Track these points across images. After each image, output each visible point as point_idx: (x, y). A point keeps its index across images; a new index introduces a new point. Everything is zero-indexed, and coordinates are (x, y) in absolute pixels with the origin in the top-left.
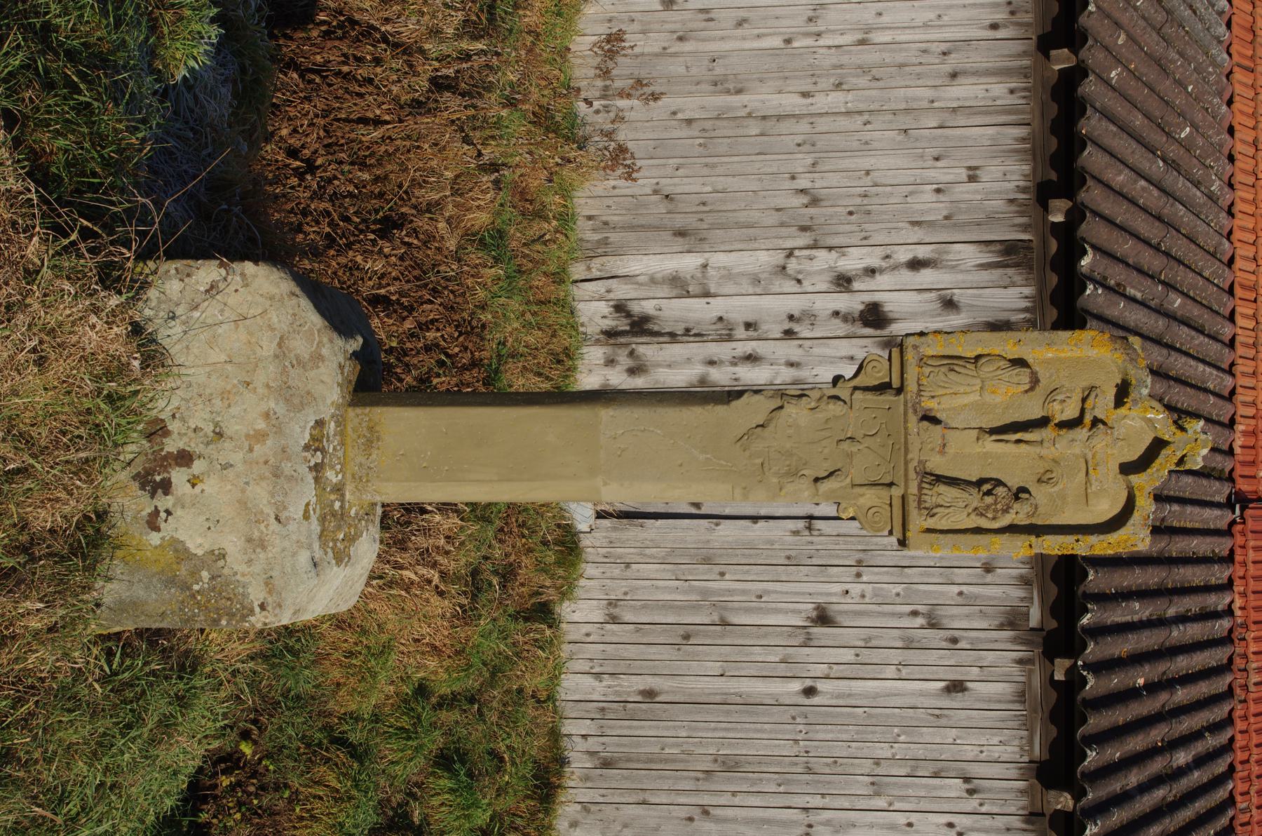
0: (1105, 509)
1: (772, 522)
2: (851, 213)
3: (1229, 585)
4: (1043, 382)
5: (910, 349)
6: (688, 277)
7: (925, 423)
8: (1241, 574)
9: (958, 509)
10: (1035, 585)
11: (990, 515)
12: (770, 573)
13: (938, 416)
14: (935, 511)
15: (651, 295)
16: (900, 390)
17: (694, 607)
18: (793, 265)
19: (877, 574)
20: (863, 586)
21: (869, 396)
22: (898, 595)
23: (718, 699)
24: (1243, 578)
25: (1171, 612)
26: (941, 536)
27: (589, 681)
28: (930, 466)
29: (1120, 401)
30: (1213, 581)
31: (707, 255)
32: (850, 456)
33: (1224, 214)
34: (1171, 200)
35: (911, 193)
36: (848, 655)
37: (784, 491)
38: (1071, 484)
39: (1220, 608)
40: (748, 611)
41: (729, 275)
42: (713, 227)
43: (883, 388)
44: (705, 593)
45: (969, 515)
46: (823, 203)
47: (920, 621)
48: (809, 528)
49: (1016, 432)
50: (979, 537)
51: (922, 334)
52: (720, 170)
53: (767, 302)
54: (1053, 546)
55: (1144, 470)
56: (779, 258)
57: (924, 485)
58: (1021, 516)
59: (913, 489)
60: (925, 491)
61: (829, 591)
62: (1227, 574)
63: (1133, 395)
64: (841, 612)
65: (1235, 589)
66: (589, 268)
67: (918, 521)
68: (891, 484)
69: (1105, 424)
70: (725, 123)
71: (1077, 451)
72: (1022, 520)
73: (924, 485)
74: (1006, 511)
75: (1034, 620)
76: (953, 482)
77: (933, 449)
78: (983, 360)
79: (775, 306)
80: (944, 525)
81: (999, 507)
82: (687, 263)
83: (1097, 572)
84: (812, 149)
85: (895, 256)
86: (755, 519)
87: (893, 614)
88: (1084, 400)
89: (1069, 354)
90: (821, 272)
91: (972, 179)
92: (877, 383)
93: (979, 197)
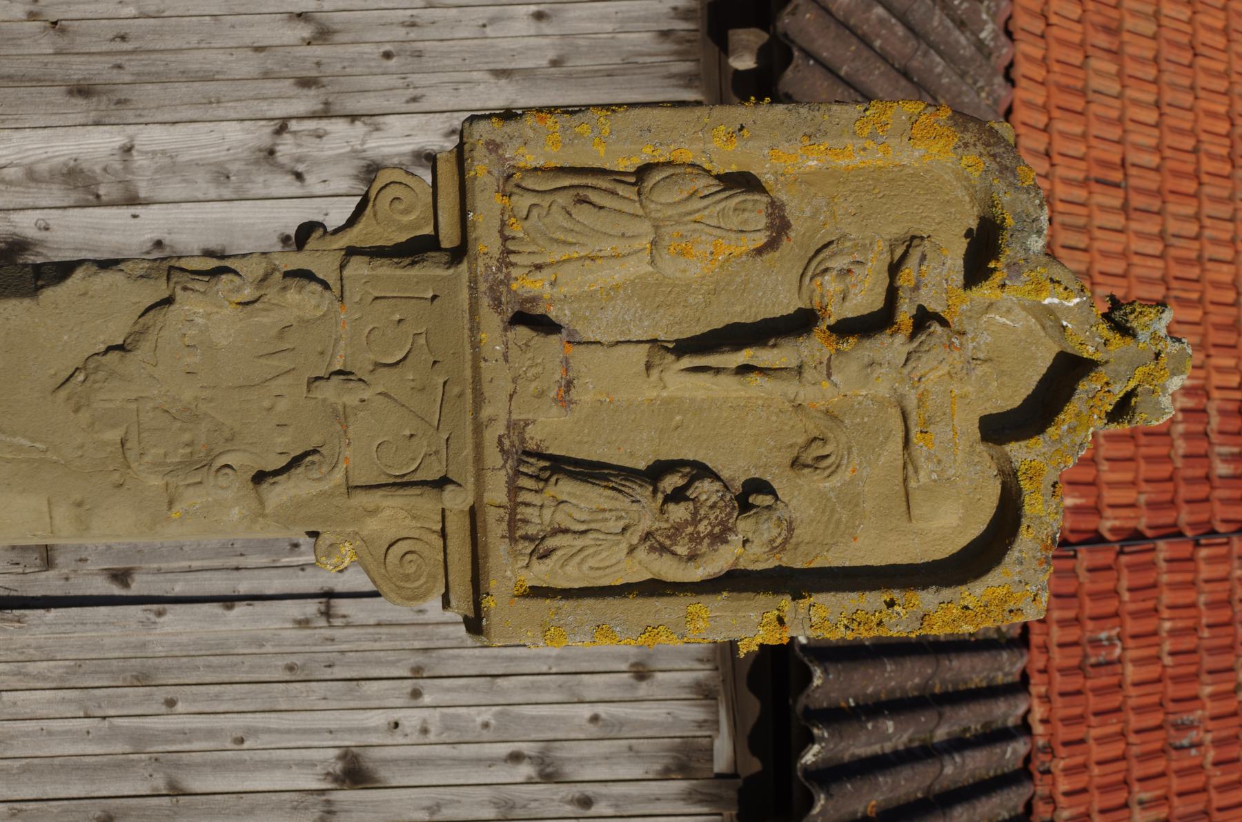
0: (950, 526)
1: (259, 606)
2: (388, 55)
3: (1022, 685)
4: (798, 228)
5: (480, 152)
6: (98, 169)
7: (523, 332)
8: (1040, 664)
9: (604, 537)
10: (722, 698)
11: (682, 550)
13: (553, 313)
14: (551, 543)
15: (29, 201)
16: (459, 254)
17: (121, 766)
18: (287, 148)
19: (449, 690)
20: (425, 713)
21: (385, 269)
22: (486, 725)
24: (1044, 671)
25: (941, 734)
26: (566, 605)
28: (536, 436)
29: (977, 268)
30: (1000, 678)
31: (131, 130)
32: (342, 416)
33: (999, 80)
34: (924, 46)
35: (493, 20)
37: (178, 508)
38: (870, 468)
39: (1011, 722)
40: (219, 767)
41: (172, 166)
42: (140, 79)
43: (416, 249)
44: (139, 739)
45: (632, 550)
46: (338, 38)
47: (525, 770)
48: (327, 614)
49: (738, 346)
50: (658, 603)
51: (508, 115)
53: (241, 213)
54: (754, 625)
55: (1041, 430)
57: (524, 482)
58: (755, 549)
59: (497, 493)
60: (525, 497)
61: (364, 724)
62: (1019, 666)
63: (1010, 252)
64: (386, 762)
65: (1034, 690)
67: (509, 570)
68: (442, 483)
69: (944, 323)
71: (882, 389)
72: (758, 558)
73: (524, 482)
74: (719, 538)
75: (722, 763)
76: (591, 472)
77: (541, 394)
78: (657, 176)
79: (261, 220)
80: (572, 577)
82: (96, 144)
83: (826, 671)
86: (229, 601)
87: (478, 761)
88: (894, 269)
89: (857, 161)
90: (337, 160)
92: (403, 238)
93: (609, 27)
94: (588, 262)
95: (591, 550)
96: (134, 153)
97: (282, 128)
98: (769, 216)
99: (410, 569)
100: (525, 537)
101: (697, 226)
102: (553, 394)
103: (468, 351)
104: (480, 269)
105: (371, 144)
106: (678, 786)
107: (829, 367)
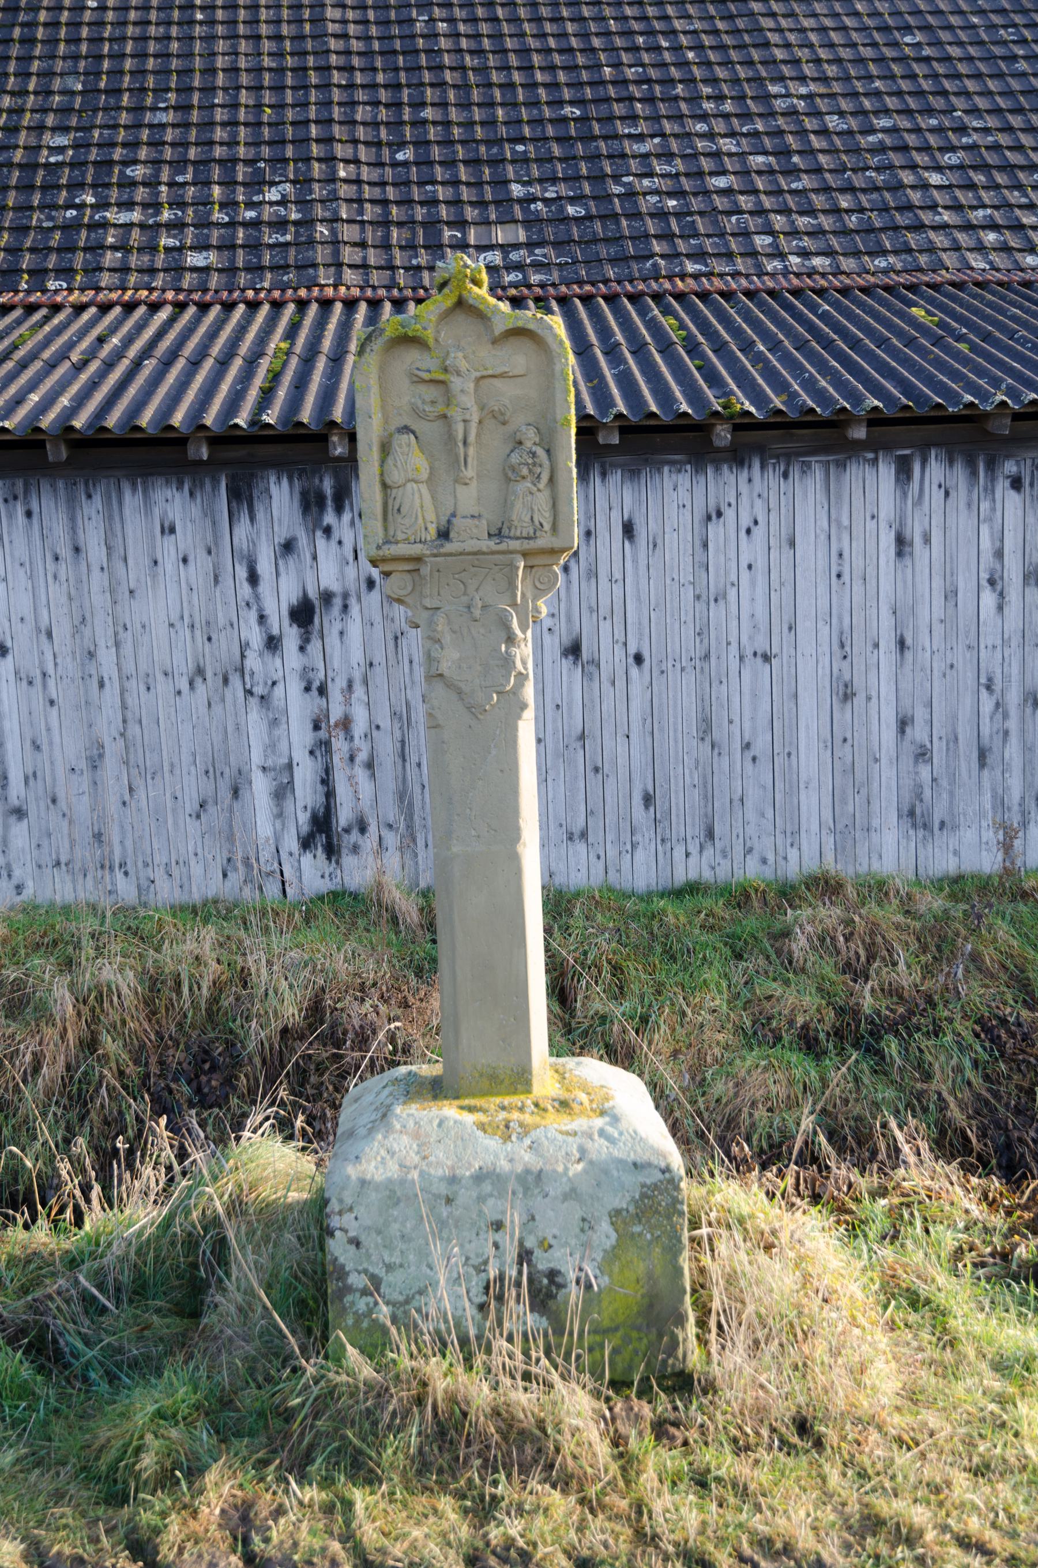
2: (209, 639)
18: (259, 690)
23: (649, 740)
27: (640, 855)
36: (605, 627)
38: (506, 392)
41: (272, 747)
52: (176, 760)
56: (254, 702)
59: (514, 545)
67: (544, 541)
70: (132, 756)
82: (261, 787)
91: (172, 530)
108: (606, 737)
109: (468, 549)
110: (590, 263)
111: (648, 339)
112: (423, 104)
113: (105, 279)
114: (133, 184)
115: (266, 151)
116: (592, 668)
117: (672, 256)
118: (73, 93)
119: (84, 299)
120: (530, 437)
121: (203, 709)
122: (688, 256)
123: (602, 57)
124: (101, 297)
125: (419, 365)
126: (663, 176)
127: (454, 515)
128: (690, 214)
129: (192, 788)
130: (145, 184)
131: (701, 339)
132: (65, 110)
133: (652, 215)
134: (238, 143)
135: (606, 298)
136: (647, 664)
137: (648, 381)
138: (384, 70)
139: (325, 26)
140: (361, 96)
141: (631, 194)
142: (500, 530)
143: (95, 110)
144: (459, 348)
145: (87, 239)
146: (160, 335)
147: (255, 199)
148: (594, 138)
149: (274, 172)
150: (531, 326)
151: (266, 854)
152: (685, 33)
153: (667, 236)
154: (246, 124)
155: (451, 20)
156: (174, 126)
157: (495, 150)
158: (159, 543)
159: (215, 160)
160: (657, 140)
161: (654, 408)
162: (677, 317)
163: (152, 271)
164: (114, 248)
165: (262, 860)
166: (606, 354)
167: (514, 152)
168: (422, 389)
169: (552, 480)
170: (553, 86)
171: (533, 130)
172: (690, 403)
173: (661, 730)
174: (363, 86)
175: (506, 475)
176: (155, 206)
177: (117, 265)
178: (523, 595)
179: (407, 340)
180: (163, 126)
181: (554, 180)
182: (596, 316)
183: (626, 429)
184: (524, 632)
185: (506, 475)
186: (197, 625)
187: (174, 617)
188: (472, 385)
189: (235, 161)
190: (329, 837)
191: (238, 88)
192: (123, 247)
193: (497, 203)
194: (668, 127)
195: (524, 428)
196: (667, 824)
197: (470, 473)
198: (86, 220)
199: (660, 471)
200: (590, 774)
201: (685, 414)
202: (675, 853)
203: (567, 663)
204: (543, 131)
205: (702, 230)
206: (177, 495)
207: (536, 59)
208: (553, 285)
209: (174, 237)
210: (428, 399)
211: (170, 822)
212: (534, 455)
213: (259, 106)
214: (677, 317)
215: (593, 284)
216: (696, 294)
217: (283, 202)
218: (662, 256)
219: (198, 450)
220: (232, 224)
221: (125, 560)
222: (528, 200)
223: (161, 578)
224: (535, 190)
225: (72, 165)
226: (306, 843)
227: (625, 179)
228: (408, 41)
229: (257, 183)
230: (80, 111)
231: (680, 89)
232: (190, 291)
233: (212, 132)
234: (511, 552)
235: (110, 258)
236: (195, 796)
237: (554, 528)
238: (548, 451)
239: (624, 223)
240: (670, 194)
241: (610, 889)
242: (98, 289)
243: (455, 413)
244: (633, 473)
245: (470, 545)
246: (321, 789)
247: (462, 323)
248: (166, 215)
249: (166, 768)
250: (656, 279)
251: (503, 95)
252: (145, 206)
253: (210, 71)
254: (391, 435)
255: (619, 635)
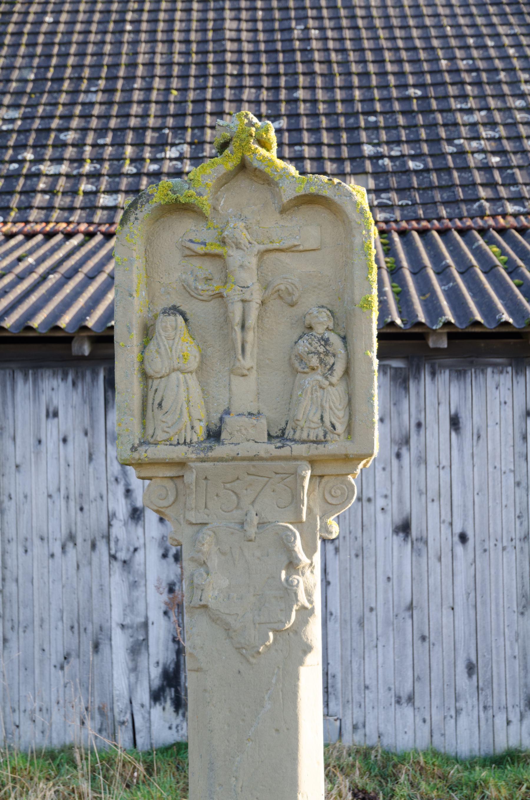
2: (81, 509)
12: (369, 570)
18: (122, 555)
20: (378, 496)
23: (472, 612)
27: (463, 720)
36: (433, 508)
38: (294, 270)
41: (130, 607)
47: (404, 451)
52: (45, 616)
56: (117, 566)
59: (299, 449)
61: (384, 524)
66: (123, 723)
67: (336, 446)
70: (7, 611)
81: (321, 349)
82: (120, 641)
84: (29, 540)
85: (116, 473)
91: (56, 414)
94: (191, 404)
95: (332, 404)
96: (124, 623)
97: (113, 557)
98: (169, 315)
99: (339, 492)
100: (325, 436)
101: (174, 351)
102: (255, 422)
103: (236, 463)
104: (194, 456)
105: (121, 517)
106: (412, 385)
107: (244, 287)
108: (433, 608)
109: (243, 453)
110: (427, 202)
111: (474, 262)
112: (296, 88)
113: (34, 215)
114: (65, 145)
115: (170, 122)
116: (421, 545)
117: (496, 200)
118: (26, 81)
119: (15, 230)
120: (322, 322)
121: (72, 571)
122: (509, 200)
123: (440, 53)
124: (28, 228)
125: (192, 236)
126: (488, 139)
127: (227, 412)
128: (511, 167)
129: (58, 641)
130: (73, 145)
131: (520, 263)
132: (19, 93)
133: (479, 169)
134: (149, 116)
135: (439, 232)
136: (470, 543)
137: (474, 296)
138: (267, 64)
139: (224, 34)
140: (247, 81)
141: (461, 153)
142: (283, 431)
143: (42, 93)
144: (241, 218)
145: (24, 185)
146: (68, 256)
147: (159, 156)
148: (432, 112)
149: (175, 136)
150: (326, 192)
151: (120, 705)
152: (507, 35)
153: (491, 184)
154: (157, 102)
155: (322, 29)
156: (101, 103)
157: (352, 120)
158: (43, 425)
159: (130, 128)
160: (483, 113)
161: (478, 317)
162: (499, 246)
163: (71, 209)
164: (44, 192)
165: (116, 710)
166: (438, 274)
167: (366, 121)
168: (196, 263)
169: (347, 372)
170: (401, 74)
171: (383, 106)
172: (511, 314)
173: (484, 603)
174: (250, 75)
175: (291, 365)
176: (80, 161)
177: (44, 204)
178: (310, 510)
179: (179, 208)
180: (92, 104)
181: (399, 142)
182: (431, 246)
183: (454, 335)
184: (310, 555)
185: (291, 365)
186: (72, 497)
187: (52, 489)
188: (254, 261)
189: (145, 128)
190: (177, 692)
191: (153, 77)
192: (51, 191)
193: (352, 159)
194: (492, 103)
195: (315, 311)
196: (489, 692)
197: (248, 362)
198: (25, 171)
199: (483, 372)
200: (418, 642)
201: (507, 323)
202: (497, 721)
203: (398, 540)
204: (391, 106)
205: (520, 180)
206: (62, 385)
207: (387, 55)
208: (396, 221)
209: (92, 184)
210: (201, 275)
211: (37, 671)
212: (326, 342)
213: (168, 90)
214: (499, 246)
215: (429, 221)
216: (516, 229)
217: (180, 158)
218: (487, 200)
219: (81, 347)
220: (138, 175)
221: (14, 439)
222: (376, 158)
223: (43, 455)
224: (384, 149)
225: (19, 132)
226: (156, 696)
227: (457, 142)
228: (287, 44)
229: (161, 144)
230: (30, 94)
231: (502, 76)
232: (99, 224)
233: (130, 107)
234: (295, 459)
235: (39, 200)
236: (60, 648)
237: (349, 430)
238: (344, 339)
239: (456, 174)
240: (494, 153)
241: (436, 753)
242: (27, 222)
243: (233, 293)
244: (459, 373)
245: (246, 449)
246: (172, 647)
247: (245, 191)
248: (87, 168)
249: (37, 623)
250: (482, 217)
251: (360, 81)
252: (72, 161)
253: (133, 65)
254: (156, 317)
255: (446, 516)
